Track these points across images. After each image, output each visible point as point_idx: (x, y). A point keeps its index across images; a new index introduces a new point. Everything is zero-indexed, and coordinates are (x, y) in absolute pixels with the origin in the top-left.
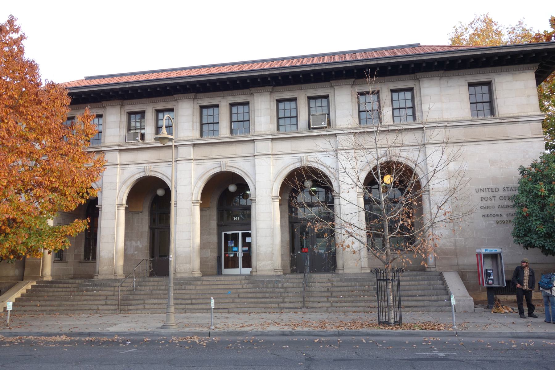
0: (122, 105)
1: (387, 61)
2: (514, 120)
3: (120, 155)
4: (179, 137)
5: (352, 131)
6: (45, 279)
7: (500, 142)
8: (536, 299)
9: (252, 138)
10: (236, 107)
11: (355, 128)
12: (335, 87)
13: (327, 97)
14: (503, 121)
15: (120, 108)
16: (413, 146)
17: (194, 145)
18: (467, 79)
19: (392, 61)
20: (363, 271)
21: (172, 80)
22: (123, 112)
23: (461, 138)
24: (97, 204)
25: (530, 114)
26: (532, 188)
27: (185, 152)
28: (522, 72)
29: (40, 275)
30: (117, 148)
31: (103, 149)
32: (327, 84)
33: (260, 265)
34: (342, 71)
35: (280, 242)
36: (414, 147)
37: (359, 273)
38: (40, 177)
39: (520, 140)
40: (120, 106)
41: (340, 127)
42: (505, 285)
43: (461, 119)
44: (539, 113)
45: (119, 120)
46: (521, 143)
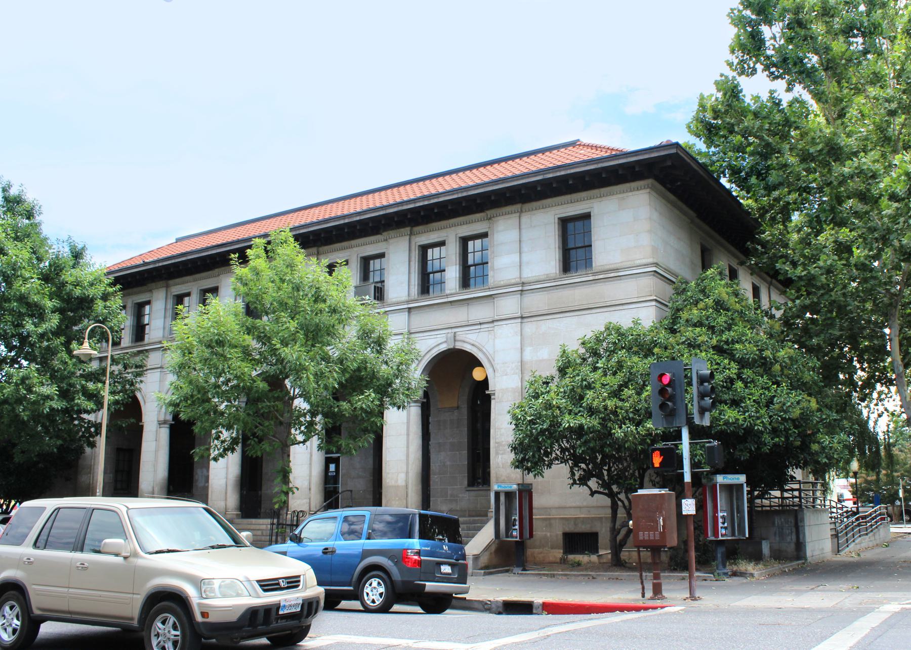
1: (460, 195)
2: (612, 275)
7: (594, 311)
10: (379, 260)
11: (555, 279)
12: (391, 241)
13: (484, 235)
14: (597, 277)
16: (480, 324)
18: (557, 212)
19: (558, 174)
21: (636, 155)
23: (544, 309)
25: (638, 262)
26: (579, 390)
27: (509, 305)
31: (146, 348)
32: (144, 288)
33: (295, 504)
34: (634, 167)
35: (166, 482)
36: (483, 326)
38: (310, 353)
39: (621, 307)
40: (518, 214)
41: (394, 300)
42: (747, 536)
43: (543, 278)
46: (623, 312)
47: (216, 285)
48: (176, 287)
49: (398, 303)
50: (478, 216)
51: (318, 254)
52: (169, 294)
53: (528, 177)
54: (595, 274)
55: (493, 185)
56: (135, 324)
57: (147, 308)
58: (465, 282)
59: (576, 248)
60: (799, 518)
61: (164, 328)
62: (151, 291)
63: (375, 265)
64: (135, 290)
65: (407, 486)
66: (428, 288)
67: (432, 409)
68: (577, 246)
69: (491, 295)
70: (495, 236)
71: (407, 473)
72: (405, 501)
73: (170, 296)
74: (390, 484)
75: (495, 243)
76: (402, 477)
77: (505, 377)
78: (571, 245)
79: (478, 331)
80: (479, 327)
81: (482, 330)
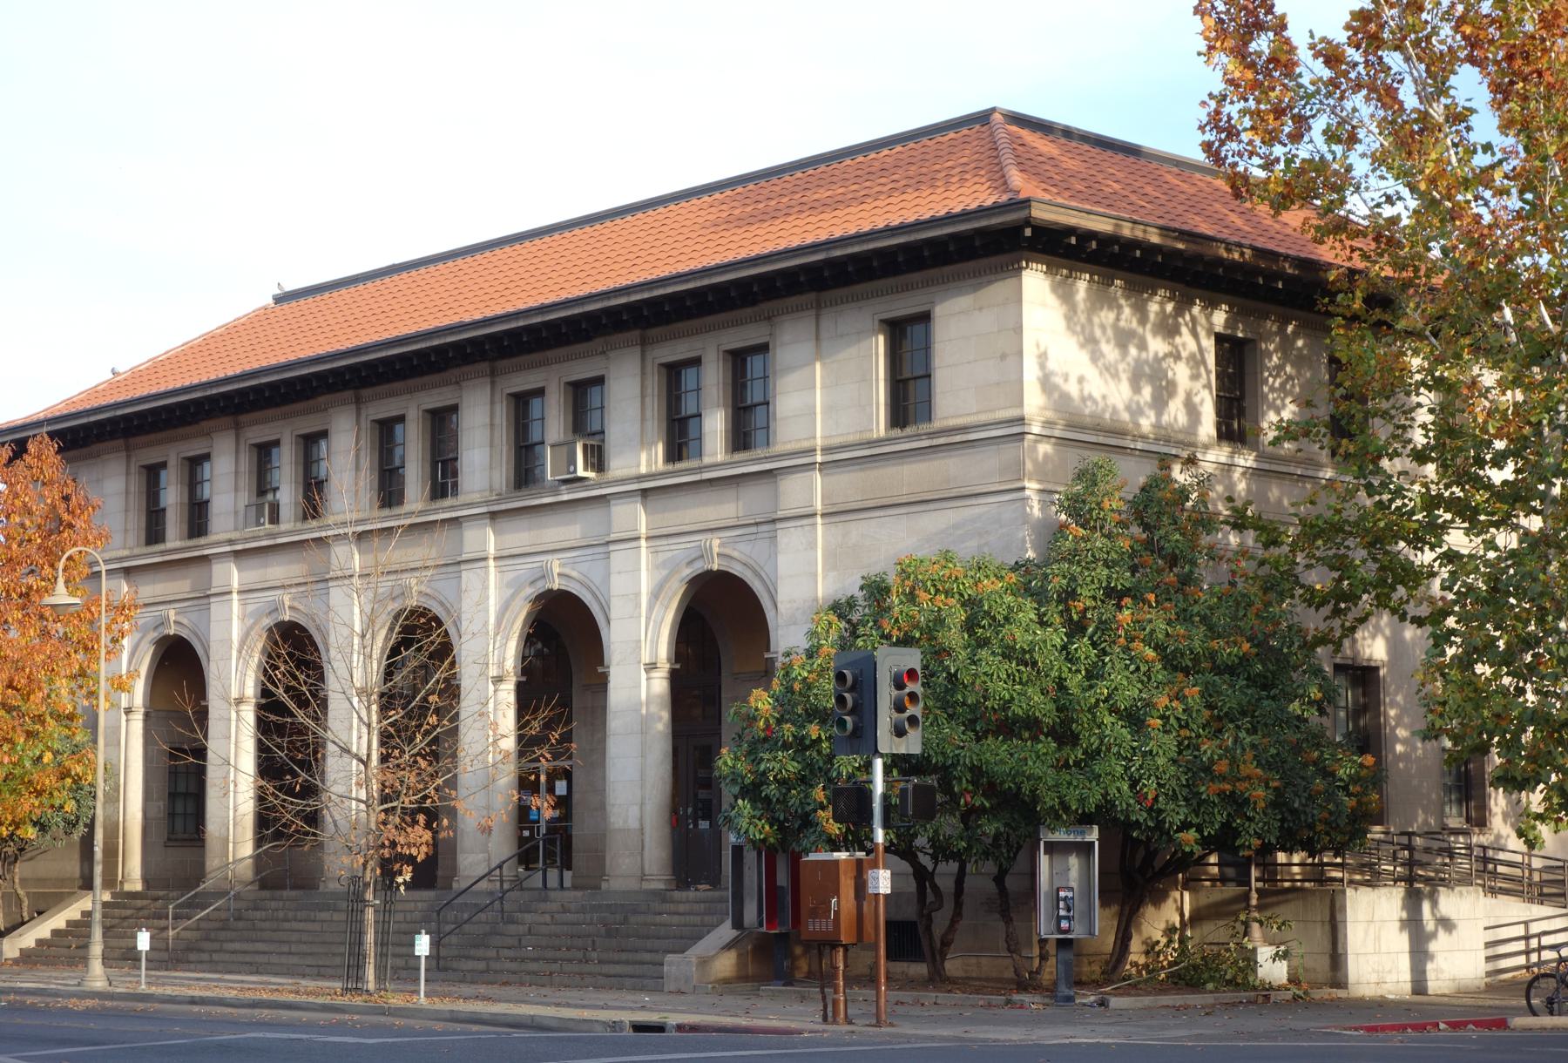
0: (493, 374)
3: (239, 571)
4: (785, 443)
5: (350, 530)
6: (127, 887)
8: (964, 975)
9: (454, 515)
10: (695, 369)
12: (612, 354)
15: (814, 321)
17: (645, 493)
19: (208, 393)
20: (646, 886)
22: (498, 397)
24: (768, 650)
27: (814, 489)
28: (993, 277)
29: (120, 878)
30: (228, 549)
31: (206, 552)
33: (466, 863)
37: (636, 892)
40: (813, 312)
44: (728, 458)
45: (487, 420)
47: (324, 428)
48: (255, 428)
49: (623, 481)
50: (749, 311)
51: (644, 343)
52: (242, 441)
53: (736, 270)
54: (931, 435)
55: (748, 267)
56: (186, 500)
57: (207, 466)
58: (740, 438)
59: (915, 378)
60: (529, 1022)
61: (236, 513)
62: (208, 434)
63: (755, 364)
64: (181, 431)
65: (642, 829)
66: (747, 435)
67: (723, 674)
68: (915, 374)
69: (770, 471)
70: (778, 351)
71: (642, 805)
72: (639, 858)
73: (133, 469)
74: (617, 826)
75: (778, 367)
76: (634, 811)
77: (792, 627)
78: (906, 374)
79: (753, 537)
80: (754, 529)
81: (760, 536)
